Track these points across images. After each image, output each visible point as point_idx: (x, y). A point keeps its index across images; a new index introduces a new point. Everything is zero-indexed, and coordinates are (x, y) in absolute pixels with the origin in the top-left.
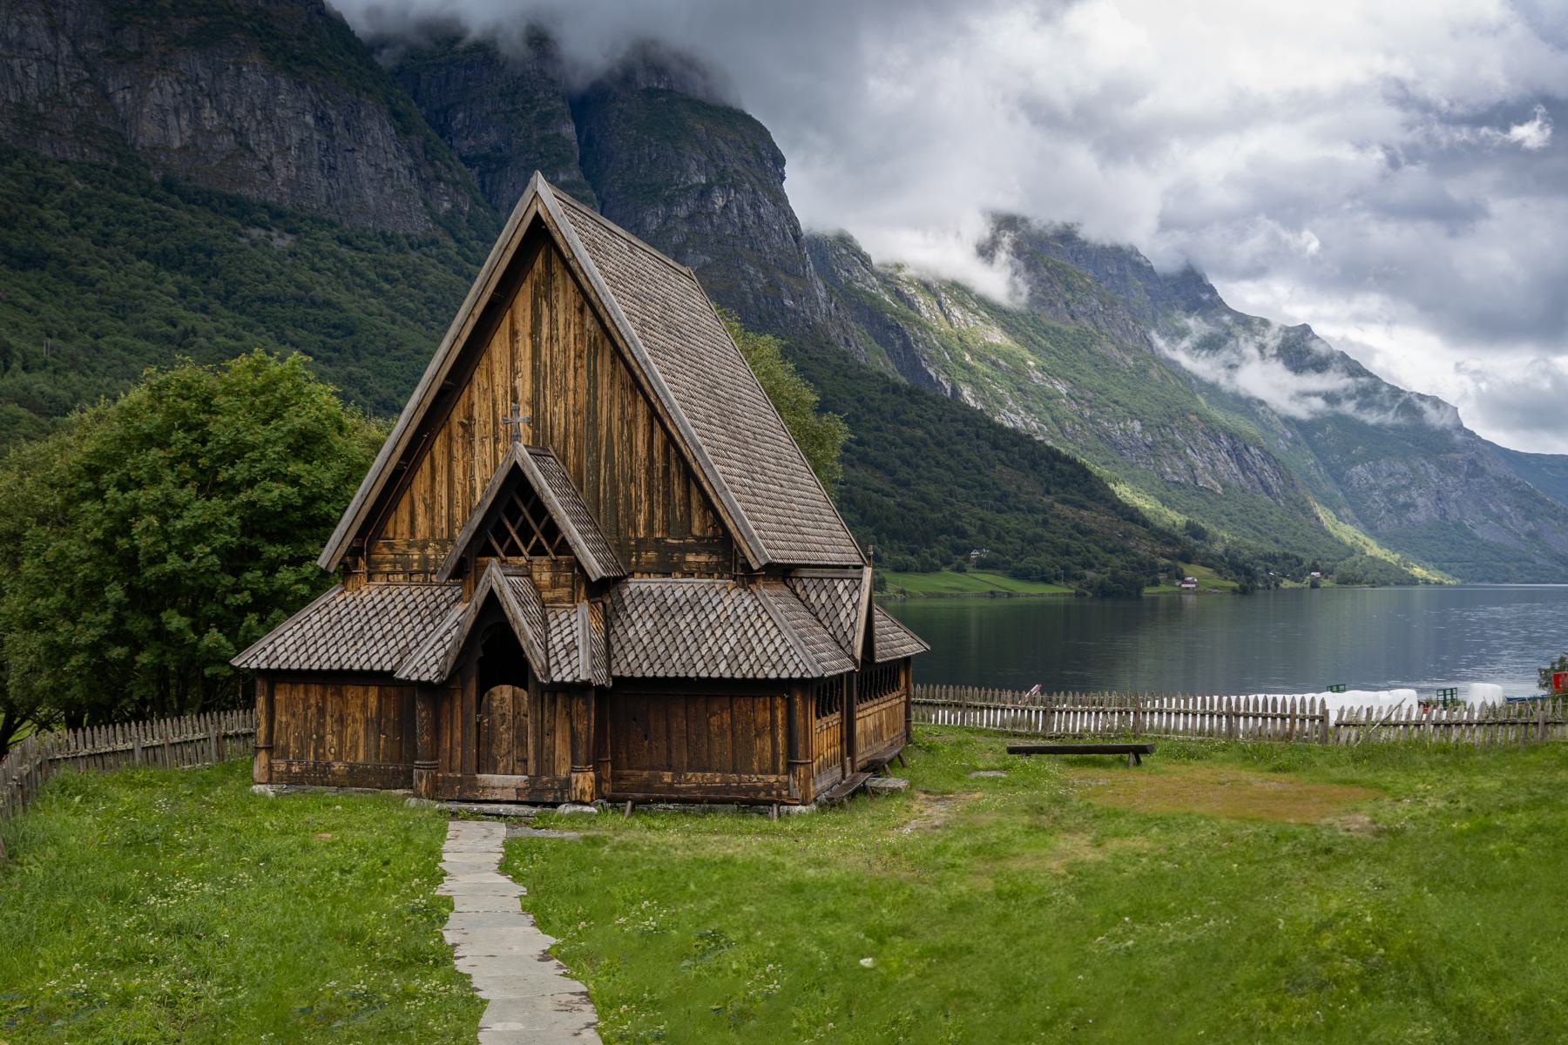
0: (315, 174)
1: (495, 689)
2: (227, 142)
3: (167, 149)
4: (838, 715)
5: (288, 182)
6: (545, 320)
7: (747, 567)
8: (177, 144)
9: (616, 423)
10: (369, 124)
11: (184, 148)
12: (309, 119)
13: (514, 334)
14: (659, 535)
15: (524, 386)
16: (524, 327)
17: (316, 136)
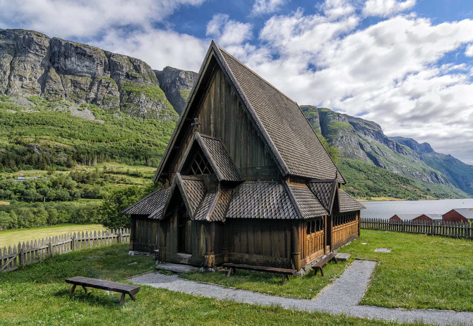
1: (188, 222)
4: (322, 231)
7: (281, 175)
13: (210, 96)
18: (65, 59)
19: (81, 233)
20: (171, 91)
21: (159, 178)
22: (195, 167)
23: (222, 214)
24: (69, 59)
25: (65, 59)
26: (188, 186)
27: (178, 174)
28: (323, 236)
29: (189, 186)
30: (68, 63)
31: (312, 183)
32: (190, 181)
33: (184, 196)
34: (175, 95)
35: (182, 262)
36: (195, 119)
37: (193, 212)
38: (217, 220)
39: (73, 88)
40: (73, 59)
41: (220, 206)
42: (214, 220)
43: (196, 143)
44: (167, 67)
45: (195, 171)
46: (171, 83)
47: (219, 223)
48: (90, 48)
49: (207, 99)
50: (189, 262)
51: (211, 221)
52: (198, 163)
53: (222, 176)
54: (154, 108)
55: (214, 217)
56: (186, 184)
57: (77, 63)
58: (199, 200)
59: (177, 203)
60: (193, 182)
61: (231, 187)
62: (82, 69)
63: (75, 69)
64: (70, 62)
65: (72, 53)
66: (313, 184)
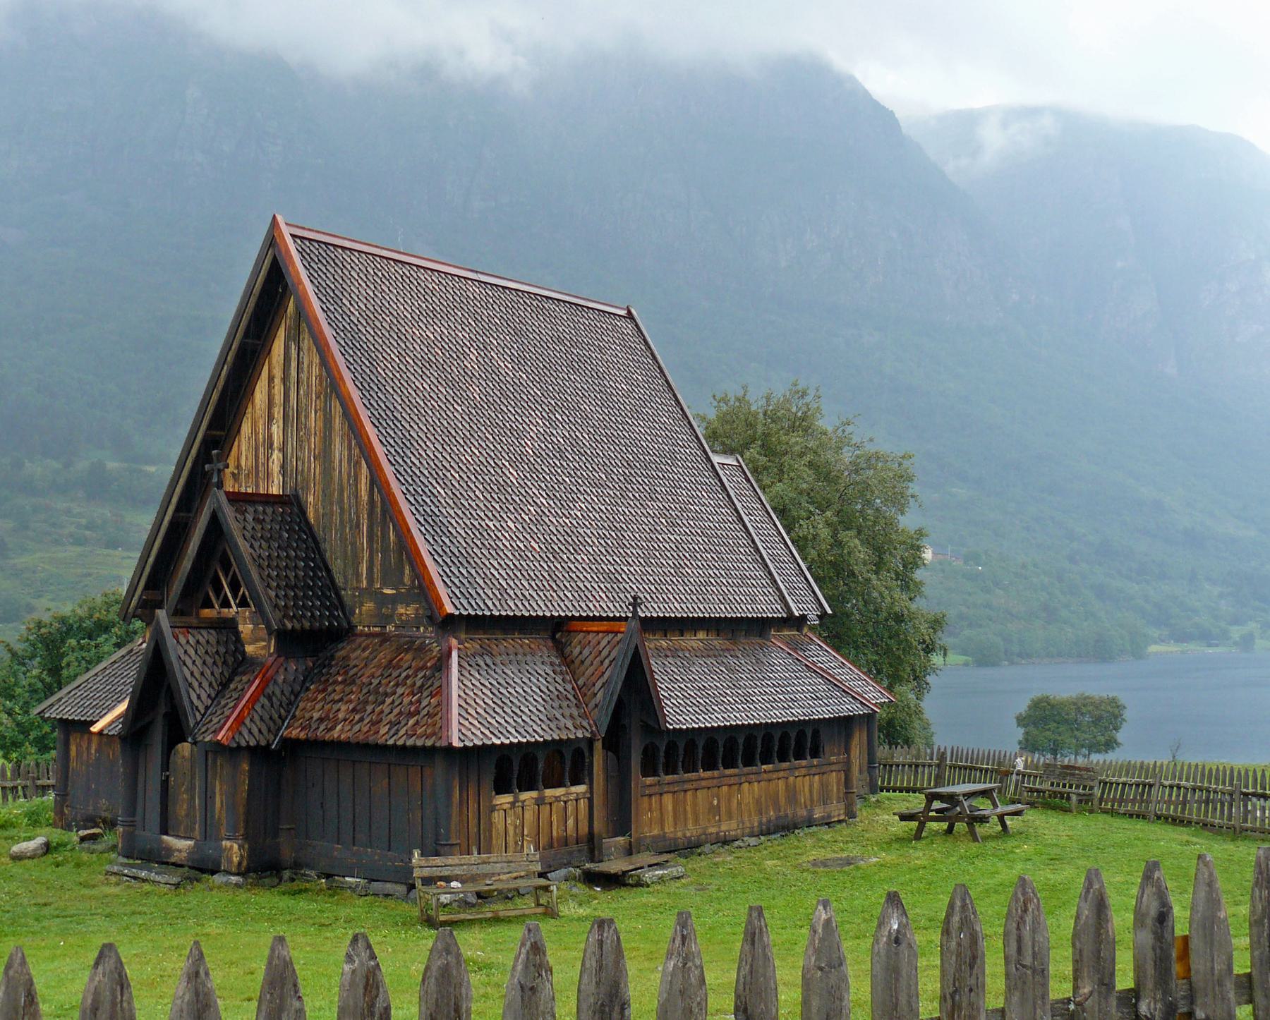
4: (581, 789)
6: (294, 364)
9: (345, 464)
13: (271, 379)
15: (276, 430)
16: (278, 373)
22: (218, 589)
28: (583, 804)
42: (244, 744)
49: (266, 367)
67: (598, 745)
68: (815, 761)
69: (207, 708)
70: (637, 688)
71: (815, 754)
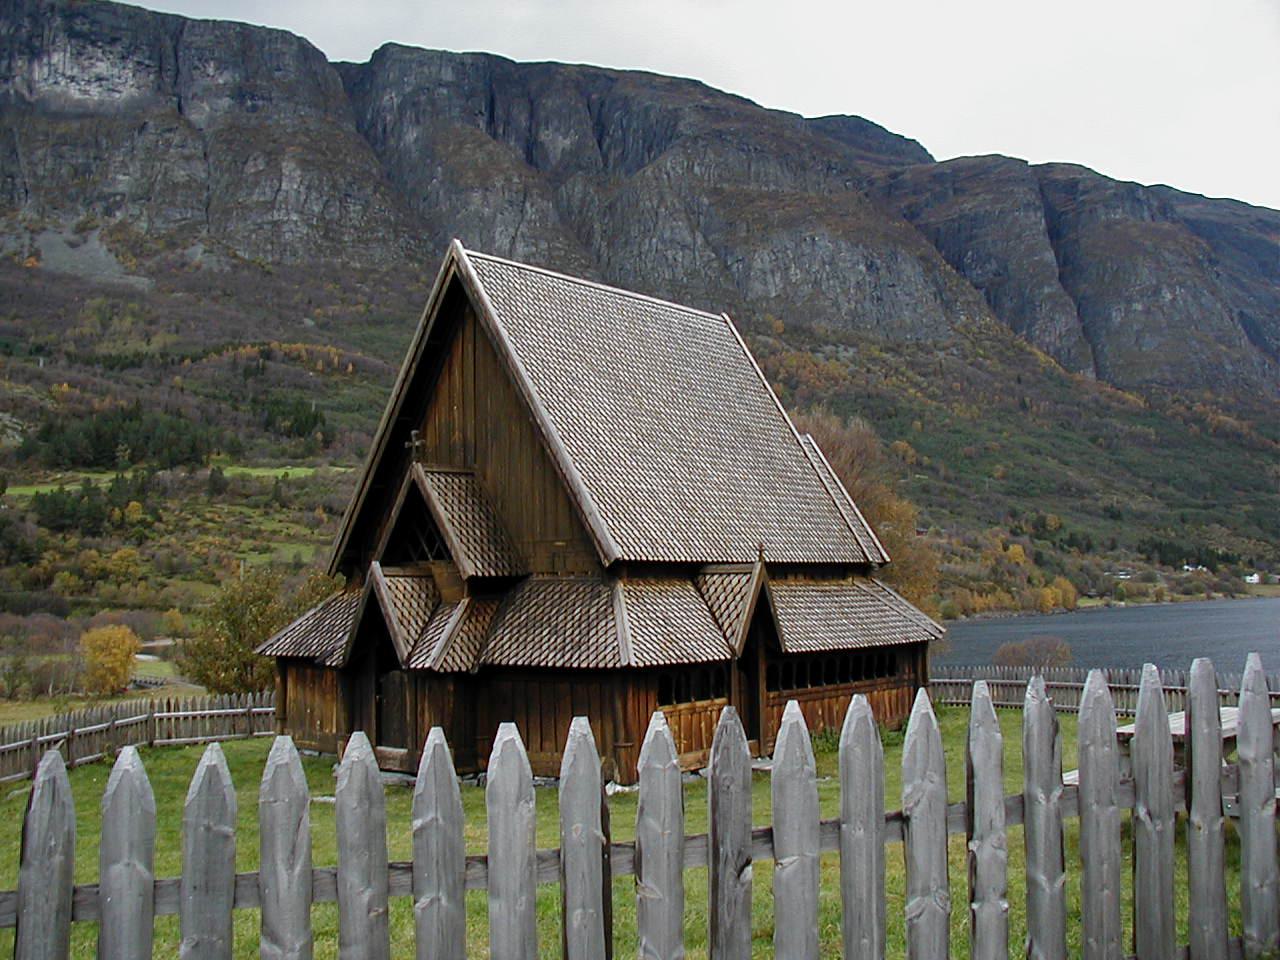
0: (867, 305)
2: (807, 289)
3: (768, 299)
5: (853, 314)
8: (774, 294)
10: (903, 266)
11: (778, 296)
12: (862, 267)
14: (550, 538)
17: (868, 279)
18: (30, 62)
19: (165, 701)
20: (400, 138)
21: (339, 565)
23: (471, 657)
24: (45, 60)
25: (30, 62)
26: (397, 592)
27: (376, 565)
29: (395, 590)
30: (39, 73)
31: (705, 575)
32: (401, 580)
33: (387, 614)
34: (415, 155)
35: (387, 767)
36: (413, 432)
37: (404, 651)
38: (456, 669)
39: (50, 161)
40: (56, 58)
41: (465, 638)
42: (449, 670)
43: (415, 490)
44: (385, 47)
45: (431, 550)
46: (399, 107)
47: (458, 677)
48: (115, 13)
50: (401, 766)
51: (442, 671)
52: (415, 540)
53: (470, 568)
54: (334, 212)
55: (450, 660)
56: (393, 587)
57: (69, 73)
58: (421, 624)
59: (372, 625)
60: (409, 580)
61: (491, 595)
62: (86, 92)
63: (58, 96)
64: (46, 69)
65: (55, 36)
66: (708, 577)
67: (734, 666)
68: (892, 679)
69: (416, 642)
70: (763, 618)
71: (892, 674)
